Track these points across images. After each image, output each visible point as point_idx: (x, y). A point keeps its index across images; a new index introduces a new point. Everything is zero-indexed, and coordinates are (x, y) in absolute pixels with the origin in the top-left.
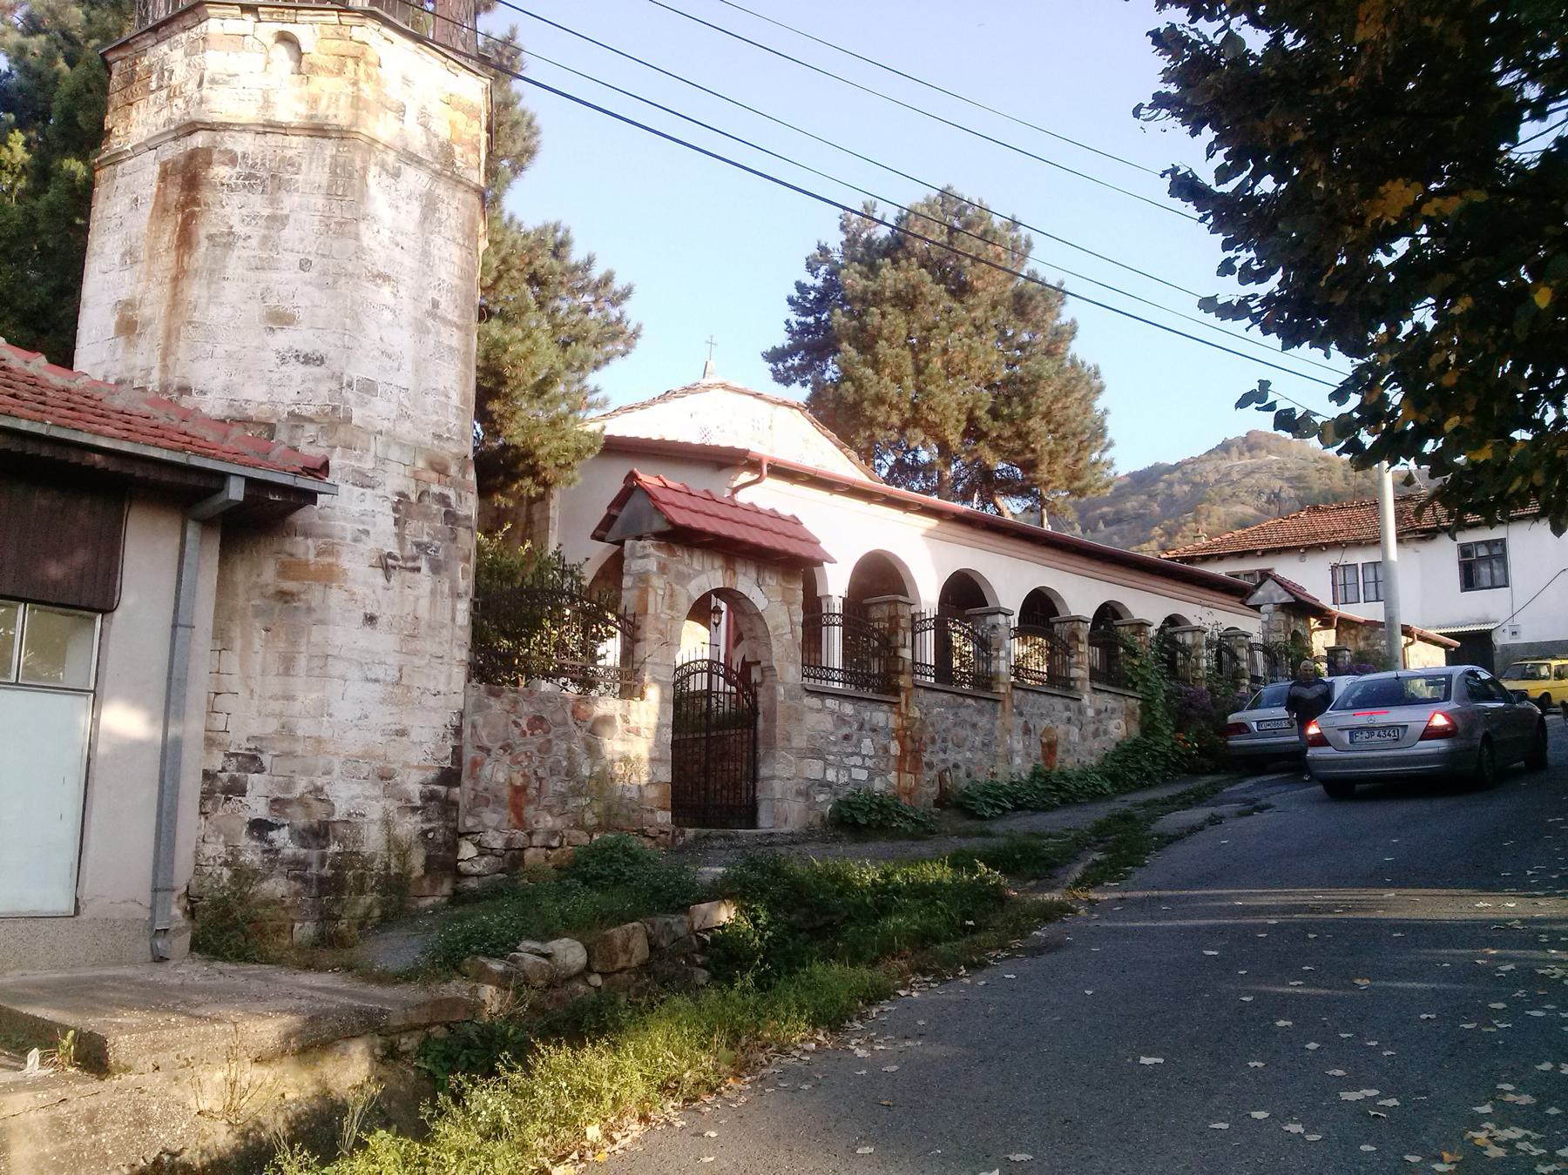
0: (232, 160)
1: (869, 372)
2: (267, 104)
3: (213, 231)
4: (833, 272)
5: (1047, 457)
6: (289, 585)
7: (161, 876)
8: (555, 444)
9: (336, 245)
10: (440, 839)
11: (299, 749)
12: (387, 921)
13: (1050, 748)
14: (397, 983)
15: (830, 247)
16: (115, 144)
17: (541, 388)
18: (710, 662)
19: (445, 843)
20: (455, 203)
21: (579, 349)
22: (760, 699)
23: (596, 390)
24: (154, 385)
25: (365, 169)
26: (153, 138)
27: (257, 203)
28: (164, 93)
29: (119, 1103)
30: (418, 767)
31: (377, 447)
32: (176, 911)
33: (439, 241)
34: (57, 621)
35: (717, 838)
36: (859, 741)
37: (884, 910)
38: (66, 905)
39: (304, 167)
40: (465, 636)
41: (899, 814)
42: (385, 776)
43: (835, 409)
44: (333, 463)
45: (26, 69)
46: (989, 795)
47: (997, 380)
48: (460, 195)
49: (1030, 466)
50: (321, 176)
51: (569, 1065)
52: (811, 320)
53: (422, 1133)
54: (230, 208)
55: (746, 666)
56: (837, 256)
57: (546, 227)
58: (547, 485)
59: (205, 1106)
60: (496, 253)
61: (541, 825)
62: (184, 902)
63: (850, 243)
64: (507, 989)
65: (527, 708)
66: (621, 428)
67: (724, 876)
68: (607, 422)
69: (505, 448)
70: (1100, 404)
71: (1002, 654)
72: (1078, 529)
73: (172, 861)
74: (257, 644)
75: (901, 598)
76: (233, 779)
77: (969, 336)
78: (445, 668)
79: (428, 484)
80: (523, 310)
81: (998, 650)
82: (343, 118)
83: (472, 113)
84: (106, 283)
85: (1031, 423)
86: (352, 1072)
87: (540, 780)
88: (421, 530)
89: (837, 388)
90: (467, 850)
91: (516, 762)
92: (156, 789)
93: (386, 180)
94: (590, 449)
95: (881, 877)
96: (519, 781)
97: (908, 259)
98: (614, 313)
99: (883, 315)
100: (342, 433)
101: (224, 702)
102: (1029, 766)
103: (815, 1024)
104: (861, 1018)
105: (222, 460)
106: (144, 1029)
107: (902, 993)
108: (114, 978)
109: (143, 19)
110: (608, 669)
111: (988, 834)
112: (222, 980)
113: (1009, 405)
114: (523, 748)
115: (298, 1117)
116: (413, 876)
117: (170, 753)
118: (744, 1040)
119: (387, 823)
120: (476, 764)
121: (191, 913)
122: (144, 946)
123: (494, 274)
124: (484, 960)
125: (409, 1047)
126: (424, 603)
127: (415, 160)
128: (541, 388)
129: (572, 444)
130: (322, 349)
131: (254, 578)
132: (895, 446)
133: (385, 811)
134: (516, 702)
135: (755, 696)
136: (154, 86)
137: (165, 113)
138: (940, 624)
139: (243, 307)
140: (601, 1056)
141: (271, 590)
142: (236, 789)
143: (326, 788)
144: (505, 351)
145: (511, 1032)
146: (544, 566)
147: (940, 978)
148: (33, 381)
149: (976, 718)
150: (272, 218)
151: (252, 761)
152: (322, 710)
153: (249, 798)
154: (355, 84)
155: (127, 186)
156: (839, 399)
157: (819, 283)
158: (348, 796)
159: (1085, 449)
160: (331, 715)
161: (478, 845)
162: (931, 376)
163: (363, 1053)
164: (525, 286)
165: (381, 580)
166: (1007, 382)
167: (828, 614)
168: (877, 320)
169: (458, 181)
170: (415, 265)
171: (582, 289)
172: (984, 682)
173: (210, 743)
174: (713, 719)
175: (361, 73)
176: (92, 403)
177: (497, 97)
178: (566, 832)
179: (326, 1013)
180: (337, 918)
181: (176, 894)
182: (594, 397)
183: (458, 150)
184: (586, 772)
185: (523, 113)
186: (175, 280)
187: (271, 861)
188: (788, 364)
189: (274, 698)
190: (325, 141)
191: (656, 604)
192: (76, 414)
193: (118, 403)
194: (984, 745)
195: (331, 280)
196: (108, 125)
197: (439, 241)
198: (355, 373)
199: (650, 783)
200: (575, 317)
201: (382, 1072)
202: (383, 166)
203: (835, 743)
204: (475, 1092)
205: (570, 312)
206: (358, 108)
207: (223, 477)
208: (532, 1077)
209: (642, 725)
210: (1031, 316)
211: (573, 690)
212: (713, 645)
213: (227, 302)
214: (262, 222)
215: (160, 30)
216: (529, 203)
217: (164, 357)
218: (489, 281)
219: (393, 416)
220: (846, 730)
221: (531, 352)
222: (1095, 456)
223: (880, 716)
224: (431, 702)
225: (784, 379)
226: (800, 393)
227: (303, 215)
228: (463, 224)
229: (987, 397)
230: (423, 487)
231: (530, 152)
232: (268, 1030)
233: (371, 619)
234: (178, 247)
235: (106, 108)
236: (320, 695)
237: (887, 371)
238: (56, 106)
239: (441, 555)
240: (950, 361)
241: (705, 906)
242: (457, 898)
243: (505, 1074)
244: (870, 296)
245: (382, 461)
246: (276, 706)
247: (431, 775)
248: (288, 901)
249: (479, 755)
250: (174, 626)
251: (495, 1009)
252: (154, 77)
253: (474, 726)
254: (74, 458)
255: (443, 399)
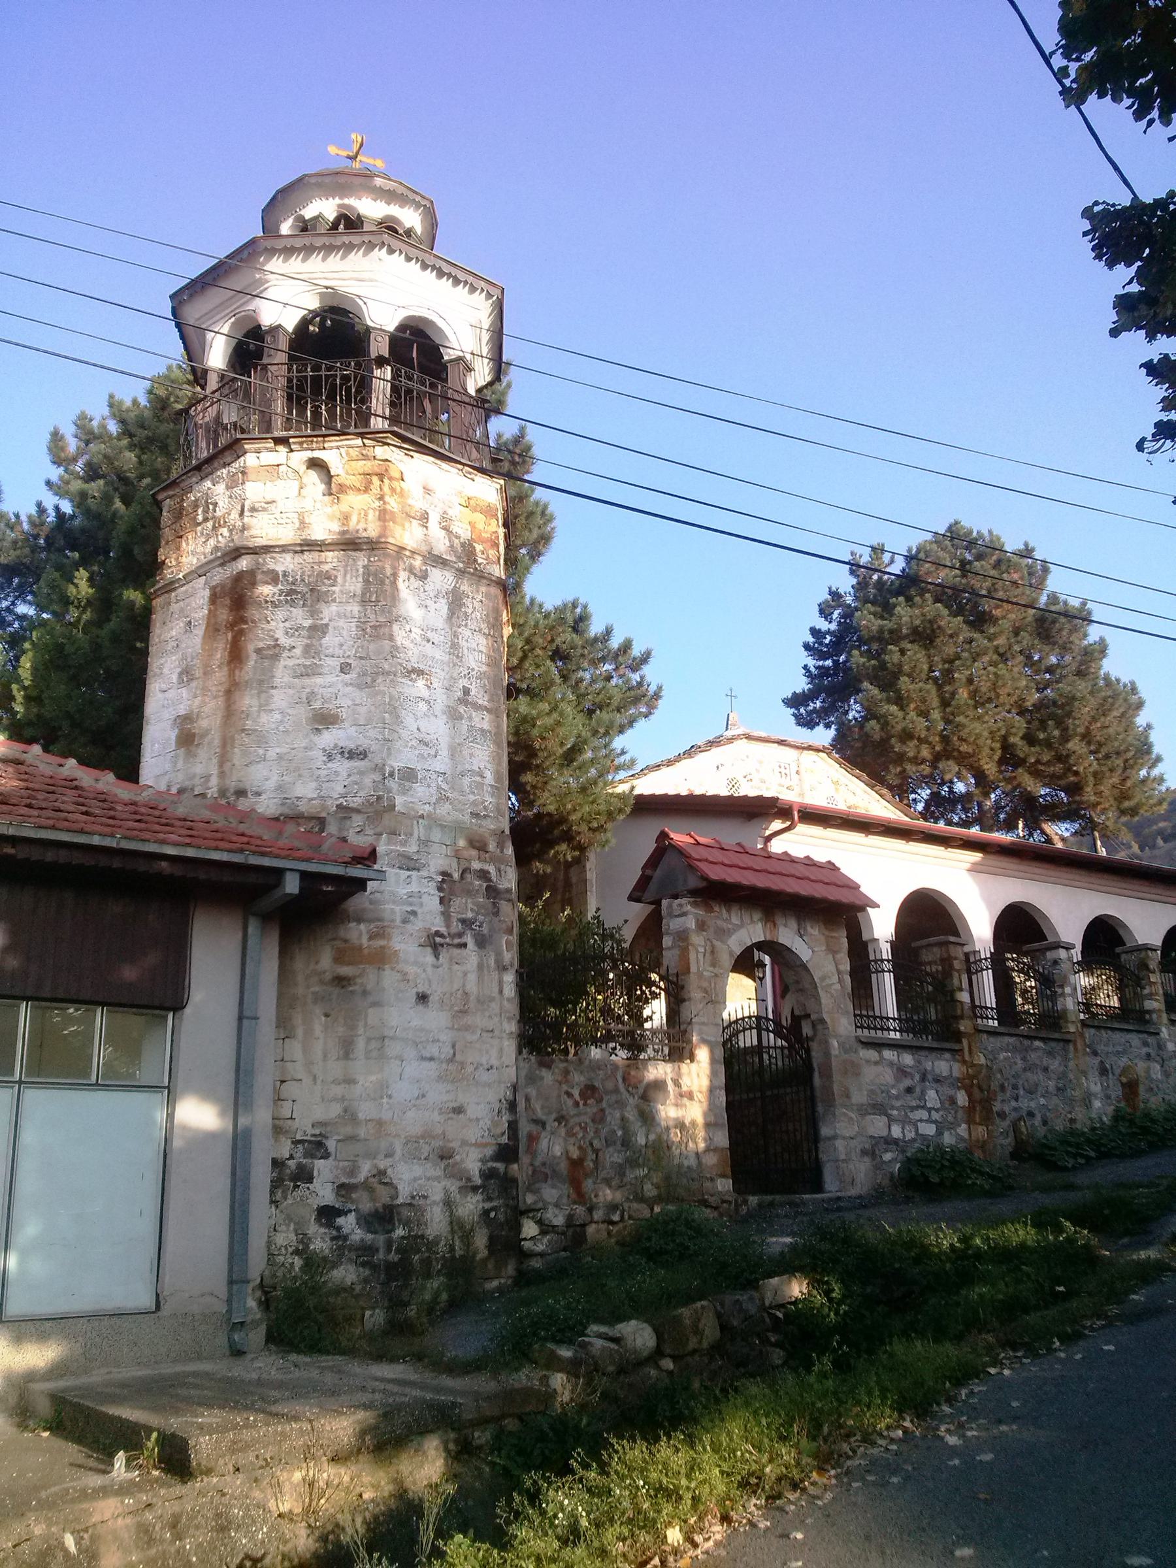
0: (274, 578)
1: (894, 708)
2: (303, 525)
3: (261, 645)
4: (848, 614)
5: (1091, 779)
6: (345, 970)
7: (236, 1268)
8: (587, 809)
9: (372, 647)
10: (501, 1217)
11: (362, 1132)
12: (455, 1306)
13: (1131, 1088)
14: (468, 1373)
15: (841, 591)
16: (168, 574)
17: (570, 756)
18: (758, 1018)
19: (507, 1221)
20: (479, 597)
21: (602, 715)
22: (813, 1054)
23: (623, 753)
24: (213, 792)
25: (395, 575)
26: (201, 566)
27: (299, 616)
28: (210, 524)
29: (202, 1507)
30: (476, 1145)
31: (419, 830)
32: (252, 1303)
33: (467, 633)
34: (133, 1021)
35: (782, 1205)
36: (923, 1093)
37: (966, 1278)
38: (146, 1301)
39: (339, 580)
40: (513, 1008)
41: (973, 1170)
42: (445, 1155)
43: (863, 748)
44: (381, 849)
45: (87, 512)
46: (1069, 1144)
47: (1029, 704)
48: (483, 589)
49: (1074, 789)
50: (355, 585)
51: (644, 1461)
52: (829, 663)
53: (501, 1540)
54: (277, 624)
55: (796, 1020)
56: (849, 600)
57: (565, 605)
58: (582, 848)
59: (285, 1507)
60: (520, 634)
61: (601, 1199)
62: (259, 1293)
63: (861, 586)
64: (577, 1377)
65: (578, 1078)
66: (648, 786)
67: (793, 1247)
68: (635, 782)
69: (539, 816)
70: (1141, 720)
71: (1068, 990)
72: (1136, 848)
73: (246, 1253)
74: (318, 1029)
75: (952, 939)
76: (300, 1166)
77: (993, 664)
78: (496, 1042)
79: (469, 861)
80: (548, 685)
81: (1062, 986)
82: (372, 530)
83: (488, 512)
84: (167, 699)
85: (1070, 745)
86: (427, 1468)
87: (596, 1152)
88: (465, 907)
89: (862, 727)
90: (530, 1229)
91: (570, 1134)
92: (229, 1181)
93: (415, 583)
94: (620, 811)
95: (959, 1241)
96: (575, 1154)
97: (922, 595)
98: (635, 677)
99: (903, 652)
100: (387, 821)
101: (290, 1089)
102: (1110, 1110)
103: (900, 1409)
104: (950, 1400)
105: (277, 856)
106: (222, 1429)
107: (993, 1371)
108: (195, 1374)
109: (187, 458)
110: (654, 1032)
111: (1070, 1187)
112: (297, 1374)
113: (1044, 729)
114: (577, 1120)
115: (376, 1517)
116: (478, 1257)
117: (240, 1143)
118: (826, 1429)
119: (448, 1204)
120: (532, 1139)
121: (265, 1304)
122: (222, 1340)
123: (520, 654)
124: (550, 1345)
125: (483, 1441)
126: (472, 977)
127: (439, 561)
128: (570, 756)
129: (602, 807)
130: (364, 743)
131: (312, 966)
132: (928, 780)
133: (447, 1193)
134: (566, 1072)
135: (808, 1051)
136: (200, 518)
137: (212, 542)
138: (997, 960)
139: (290, 711)
140: (677, 1450)
141: (328, 976)
142: (304, 1176)
143: (389, 1171)
144: (534, 726)
145: (584, 1421)
146: (585, 931)
147: (1031, 1352)
148: (103, 798)
149: (1046, 1061)
150: (313, 628)
151: (317, 1147)
152: (382, 1091)
153: (316, 1185)
154: (381, 498)
155: (182, 610)
156: (866, 738)
157: (833, 626)
158: (410, 1177)
159: (1132, 767)
160: (390, 1097)
161: (540, 1222)
162: (958, 707)
163: (436, 1449)
164: (548, 662)
165: (429, 958)
166: (1039, 706)
167: (876, 961)
168: (896, 657)
169: (480, 576)
170: (446, 658)
171: (603, 660)
172: (1051, 1022)
173: (278, 1131)
174: (767, 1076)
175: (386, 489)
176: (157, 813)
177: (512, 492)
178: (626, 1206)
179: (399, 1407)
180: (406, 1305)
181: (251, 1285)
182: (622, 759)
183: (479, 548)
184: (641, 1140)
185: (537, 503)
186: (229, 693)
187: (339, 1248)
188: (810, 708)
189: (336, 1082)
190: (357, 554)
191: (698, 961)
192: (143, 825)
193: (181, 811)
194: (1059, 1089)
195: (368, 681)
196: (161, 557)
197: (467, 633)
198: (396, 763)
199: (707, 1150)
200: (598, 686)
201: (458, 1468)
202: (411, 570)
203: (897, 1098)
204: (551, 1493)
205: (593, 681)
206: (385, 521)
207: (279, 872)
208: (608, 1474)
209: (695, 1089)
210: (1057, 638)
211: (623, 1054)
212: (760, 1000)
213: (277, 710)
214: (304, 633)
215: (205, 468)
216: (546, 586)
217: (221, 764)
218: (515, 661)
219: (433, 800)
220: (907, 1082)
221: (558, 723)
222: (1143, 773)
223: (943, 1066)
224: (485, 1077)
225: (807, 722)
226: (824, 735)
227: (341, 623)
228: (487, 616)
229: (1020, 723)
230: (464, 864)
231: (545, 539)
232: (343, 1427)
233: (423, 998)
234: (230, 662)
235: (160, 542)
236: (379, 1076)
237: (912, 706)
238: (114, 543)
239: (485, 930)
240: (976, 691)
241: (775, 1281)
242: (524, 1278)
243: (581, 1473)
244: (886, 635)
245: (425, 843)
246: (338, 1090)
247: (489, 1151)
248: (358, 1288)
249: (534, 1129)
250: (241, 1018)
251: (566, 1397)
252: (200, 511)
253: (528, 1099)
254: (142, 866)
255: (478, 779)
